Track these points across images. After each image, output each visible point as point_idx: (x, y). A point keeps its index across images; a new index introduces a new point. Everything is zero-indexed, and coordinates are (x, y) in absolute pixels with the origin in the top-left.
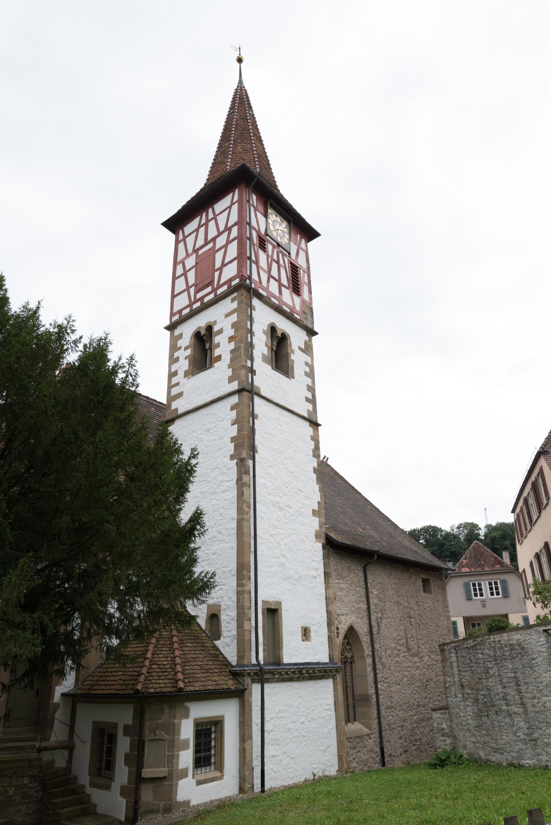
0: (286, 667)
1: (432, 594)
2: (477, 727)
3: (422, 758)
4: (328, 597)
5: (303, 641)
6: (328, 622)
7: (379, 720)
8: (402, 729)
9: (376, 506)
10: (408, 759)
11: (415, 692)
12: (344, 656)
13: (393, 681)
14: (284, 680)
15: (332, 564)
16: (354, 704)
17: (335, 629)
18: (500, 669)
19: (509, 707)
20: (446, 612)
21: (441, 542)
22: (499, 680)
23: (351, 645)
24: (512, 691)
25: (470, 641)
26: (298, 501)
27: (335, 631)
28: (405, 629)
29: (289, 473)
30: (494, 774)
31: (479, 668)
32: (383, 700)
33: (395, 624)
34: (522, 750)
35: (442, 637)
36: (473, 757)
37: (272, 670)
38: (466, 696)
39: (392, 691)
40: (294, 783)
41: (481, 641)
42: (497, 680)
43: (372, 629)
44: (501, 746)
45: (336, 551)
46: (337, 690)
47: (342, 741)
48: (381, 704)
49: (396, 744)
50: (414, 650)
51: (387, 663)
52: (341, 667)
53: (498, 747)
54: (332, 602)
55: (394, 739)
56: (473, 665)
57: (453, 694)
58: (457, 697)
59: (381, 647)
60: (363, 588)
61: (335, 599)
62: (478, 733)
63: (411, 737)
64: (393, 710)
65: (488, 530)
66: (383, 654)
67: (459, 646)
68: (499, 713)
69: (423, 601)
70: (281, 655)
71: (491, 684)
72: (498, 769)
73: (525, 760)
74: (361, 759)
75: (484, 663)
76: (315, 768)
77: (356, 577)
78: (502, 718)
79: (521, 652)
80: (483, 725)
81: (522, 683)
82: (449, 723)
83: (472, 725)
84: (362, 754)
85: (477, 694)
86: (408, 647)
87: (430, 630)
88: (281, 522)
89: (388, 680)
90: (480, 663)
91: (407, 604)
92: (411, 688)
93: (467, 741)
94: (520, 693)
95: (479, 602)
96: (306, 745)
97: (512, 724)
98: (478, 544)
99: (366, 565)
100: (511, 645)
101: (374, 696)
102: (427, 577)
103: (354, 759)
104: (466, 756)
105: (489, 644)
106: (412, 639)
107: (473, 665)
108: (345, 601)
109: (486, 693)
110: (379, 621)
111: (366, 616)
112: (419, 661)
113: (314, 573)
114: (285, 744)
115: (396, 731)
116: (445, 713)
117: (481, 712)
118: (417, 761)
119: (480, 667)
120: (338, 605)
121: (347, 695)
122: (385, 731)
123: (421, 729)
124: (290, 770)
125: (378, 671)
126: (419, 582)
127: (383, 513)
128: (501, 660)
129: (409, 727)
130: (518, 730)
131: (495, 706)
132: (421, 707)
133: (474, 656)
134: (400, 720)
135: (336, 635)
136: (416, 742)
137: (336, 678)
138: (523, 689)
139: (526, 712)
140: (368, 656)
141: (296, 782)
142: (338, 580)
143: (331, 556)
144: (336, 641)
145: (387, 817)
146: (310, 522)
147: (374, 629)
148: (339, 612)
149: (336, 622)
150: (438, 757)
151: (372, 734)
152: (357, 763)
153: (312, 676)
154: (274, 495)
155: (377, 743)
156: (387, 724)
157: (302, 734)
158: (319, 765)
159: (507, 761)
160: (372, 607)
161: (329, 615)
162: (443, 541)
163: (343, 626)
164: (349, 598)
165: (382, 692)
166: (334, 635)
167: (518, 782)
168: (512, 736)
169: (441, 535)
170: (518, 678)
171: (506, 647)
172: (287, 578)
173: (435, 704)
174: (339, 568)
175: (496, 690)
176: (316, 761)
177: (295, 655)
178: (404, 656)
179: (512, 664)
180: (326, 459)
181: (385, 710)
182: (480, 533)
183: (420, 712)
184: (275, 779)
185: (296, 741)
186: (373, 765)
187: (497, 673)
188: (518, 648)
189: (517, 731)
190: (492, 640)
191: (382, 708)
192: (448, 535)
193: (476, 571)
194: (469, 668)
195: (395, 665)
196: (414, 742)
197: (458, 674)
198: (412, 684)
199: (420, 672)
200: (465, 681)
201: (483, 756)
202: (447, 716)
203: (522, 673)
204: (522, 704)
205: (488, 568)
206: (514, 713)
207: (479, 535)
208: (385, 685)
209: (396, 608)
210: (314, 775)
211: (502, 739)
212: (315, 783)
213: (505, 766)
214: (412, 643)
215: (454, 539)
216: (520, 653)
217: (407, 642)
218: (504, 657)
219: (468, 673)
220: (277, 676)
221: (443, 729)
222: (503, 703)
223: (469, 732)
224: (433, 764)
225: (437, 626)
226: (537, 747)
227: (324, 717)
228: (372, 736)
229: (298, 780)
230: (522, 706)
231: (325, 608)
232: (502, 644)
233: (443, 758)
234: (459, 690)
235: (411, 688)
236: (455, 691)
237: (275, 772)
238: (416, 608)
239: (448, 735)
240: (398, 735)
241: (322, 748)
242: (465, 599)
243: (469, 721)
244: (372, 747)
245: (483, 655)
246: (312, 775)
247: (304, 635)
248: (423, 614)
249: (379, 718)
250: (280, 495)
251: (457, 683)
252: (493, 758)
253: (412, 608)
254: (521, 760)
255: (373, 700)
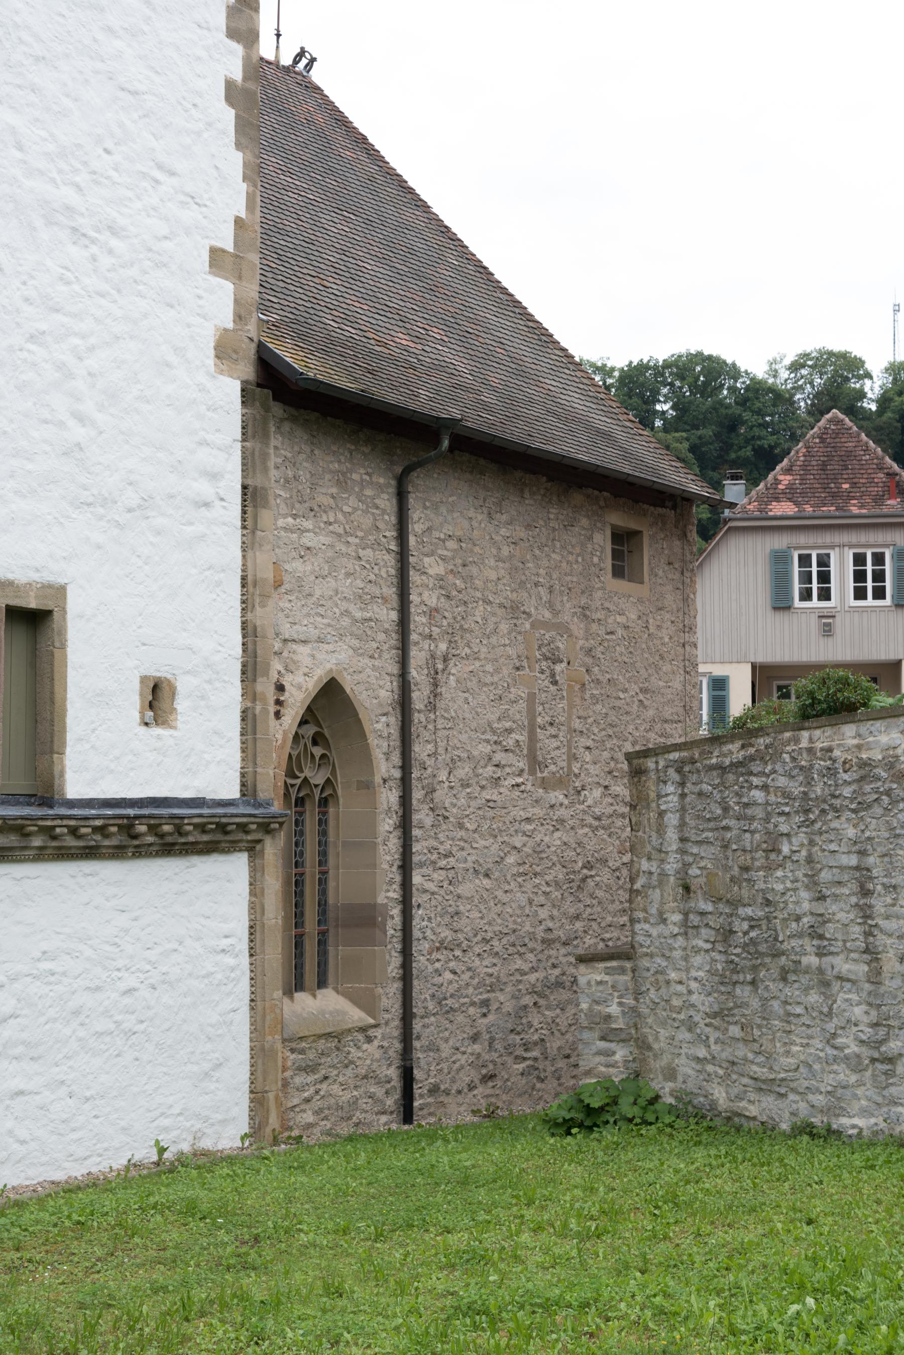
0: (75, 812)
1: (642, 582)
2: (715, 1015)
3: (540, 1098)
4: (250, 578)
5: (146, 724)
6: (244, 665)
7: (405, 985)
8: (485, 1010)
9: (479, 256)
10: (493, 1100)
11: (542, 899)
12: (298, 781)
13: (469, 865)
14: (63, 855)
15: (273, 460)
16: (323, 934)
17: (272, 689)
18: (817, 839)
19: (824, 959)
20: (684, 645)
21: (730, 412)
22: (806, 875)
23: (327, 746)
24: (842, 910)
25: (730, 746)
26: (154, 209)
27: (271, 694)
28: (531, 698)
29: (121, 94)
30: (740, 1157)
31: (748, 835)
32: (425, 923)
33: (496, 679)
34: (844, 1087)
35: (658, 727)
36: (690, 1102)
37: (19, 822)
38: (694, 919)
39: (459, 897)
40: (89, 1174)
41: (767, 747)
42: (799, 874)
43: (410, 691)
44: (782, 1075)
45: (294, 411)
46: (263, 889)
47: (267, 1046)
48: (416, 934)
49: (459, 1056)
50: (552, 768)
51: (454, 805)
52: (281, 816)
53: (772, 1076)
54: (265, 596)
55: (451, 1043)
56: (732, 823)
57: (654, 911)
58: (664, 921)
59: (435, 753)
60: (389, 551)
61: (278, 584)
62: (718, 1034)
63: (512, 1036)
64: (458, 953)
65: (895, 380)
66: (443, 775)
67: (693, 762)
68: (792, 977)
69: (607, 605)
70: (57, 770)
71: (779, 887)
72: (762, 1139)
73: (850, 1117)
74: (333, 1101)
75: (767, 820)
76: (166, 1129)
77: (365, 512)
78: (797, 993)
79: (891, 789)
80: (736, 1011)
81: (879, 887)
82: (629, 1001)
83: (702, 1008)
84: (336, 1086)
85: (731, 915)
86: (535, 757)
87: (618, 703)
88: (76, 287)
89: (451, 859)
90: (753, 818)
91: (548, 615)
92: (528, 886)
93: (680, 1054)
94: (866, 917)
95: (814, 618)
96: (137, 1059)
97: (825, 1010)
98: (840, 422)
99: (408, 470)
100: (864, 764)
101: (396, 912)
102: (633, 525)
103: (307, 1100)
104: (670, 1100)
105: (794, 759)
106: (552, 730)
107: (732, 823)
108: (318, 593)
109: (760, 914)
110: (440, 666)
111: (391, 648)
112: (566, 802)
113: (205, 489)
114: (61, 1056)
115: (460, 1018)
116: (623, 971)
117: (735, 971)
118: (523, 1107)
119: (753, 832)
120: (288, 605)
121: (299, 905)
122: (422, 1017)
123: (547, 1013)
124: (74, 1136)
125: (416, 832)
126: (603, 541)
127: (505, 284)
128: (823, 811)
129: (508, 1007)
130: (843, 1028)
131: (783, 953)
132: (558, 945)
133: (737, 794)
134: (482, 984)
135: (272, 709)
136: (526, 1050)
137: (262, 851)
138: (879, 904)
139: (875, 976)
140: (385, 781)
141: (94, 1170)
142: (295, 516)
143: (273, 429)
144: (271, 730)
145: (353, 1292)
146: (200, 297)
147: (415, 695)
148: (287, 631)
149: (277, 665)
150: (581, 1101)
151: (375, 1026)
152: (316, 1113)
153: (174, 844)
154: (53, 181)
155: (391, 1053)
156: (433, 996)
157: (125, 1026)
158: (181, 1118)
159: (794, 1119)
160: (418, 620)
161: (250, 639)
162: (738, 410)
163: (299, 678)
164: (333, 584)
165: (426, 897)
166: (265, 710)
167: (809, 1185)
168: (820, 1046)
169: (733, 390)
170: (868, 870)
171: (845, 772)
172: (91, 499)
173: (607, 936)
174: (304, 475)
175: (791, 906)
176: (171, 1106)
177: (112, 772)
178: (518, 785)
179: (855, 826)
180: (304, 62)
181: (430, 954)
182: (867, 389)
183: (553, 960)
184: (19, 1162)
185: (102, 1046)
186: (369, 1117)
187: (804, 853)
188: (884, 774)
189: (839, 1032)
190: (804, 744)
191: (420, 948)
192: (757, 388)
193: (817, 514)
194: (716, 834)
195: (481, 812)
196: (520, 1052)
197: (676, 852)
198: (535, 874)
199: (565, 839)
200: (698, 872)
201: (721, 1101)
202: (627, 978)
203: (885, 855)
204: (866, 951)
205: (862, 507)
206: (839, 978)
207: (861, 395)
208: (437, 876)
209: (504, 627)
210: (162, 1151)
211: (788, 1053)
212: (159, 1174)
213: (784, 1133)
214: (547, 743)
215: (774, 405)
216: (888, 793)
217: (532, 739)
218: (833, 801)
219: (712, 849)
220: (37, 842)
221: (608, 1018)
222: (809, 945)
223: (690, 1030)
224: (560, 1120)
225: (644, 691)
226: (891, 1081)
227: (209, 975)
228: (378, 1033)
229: (104, 1166)
230: (867, 957)
231: (238, 613)
232: (834, 761)
233: (596, 1104)
234: (676, 901)
235: (528, 886)
236: (662, 903)
237: (23, 1142)
238: (577, 627)
239: (623, 1036)
240: (467, 1029)
241: (195, 1068)
242: (769, 607)
243: (694, 998)
244: (374, 1067)
245: (768, 793)
246: (155, 1151)
247: (151, 706)
248: (601, 649)
249: (406, 977)
250: (78, 179)
251: (672, 879)
252: (751, 1108)
253: (563, 629)
254: (837, 1116)
255: (390, 923)
